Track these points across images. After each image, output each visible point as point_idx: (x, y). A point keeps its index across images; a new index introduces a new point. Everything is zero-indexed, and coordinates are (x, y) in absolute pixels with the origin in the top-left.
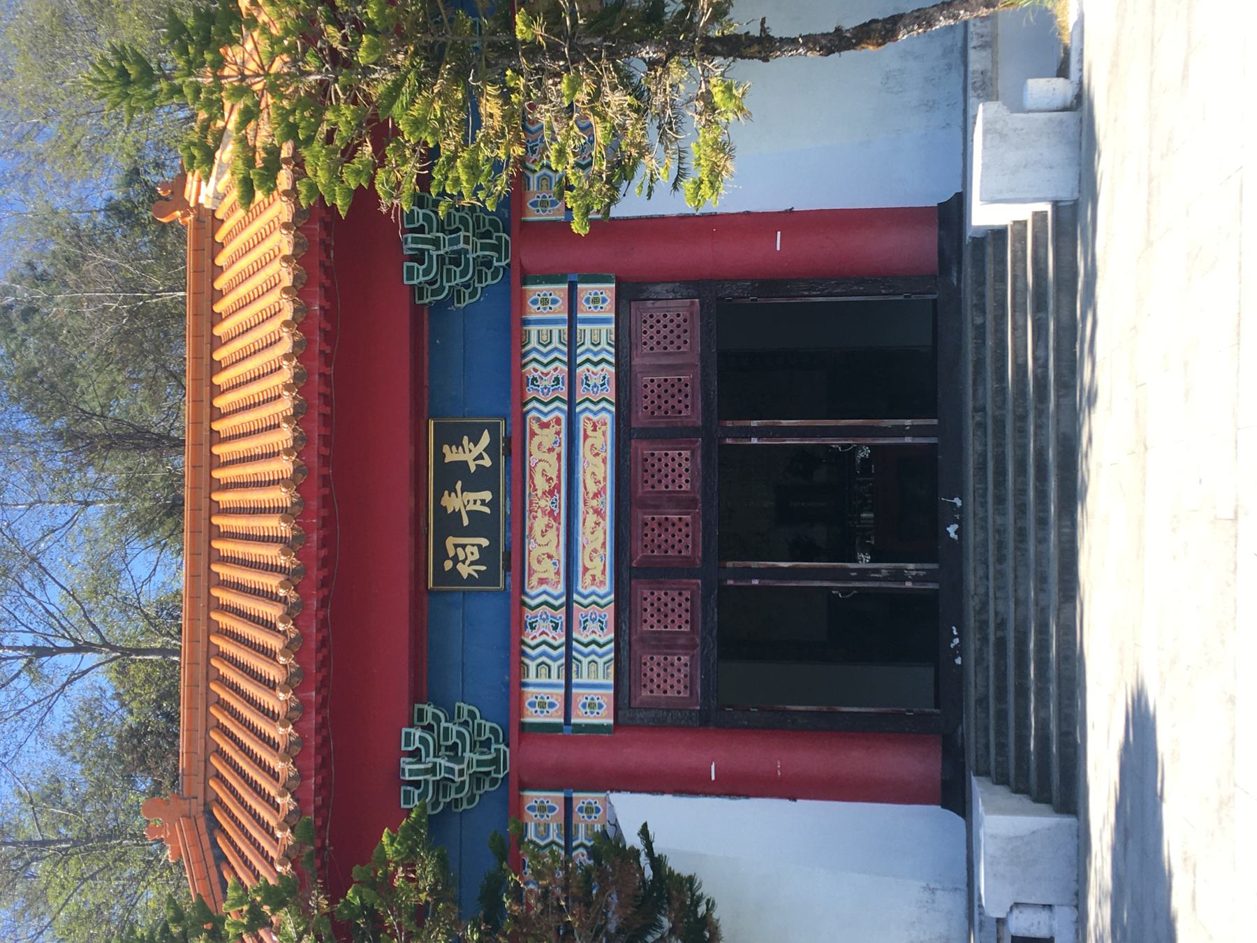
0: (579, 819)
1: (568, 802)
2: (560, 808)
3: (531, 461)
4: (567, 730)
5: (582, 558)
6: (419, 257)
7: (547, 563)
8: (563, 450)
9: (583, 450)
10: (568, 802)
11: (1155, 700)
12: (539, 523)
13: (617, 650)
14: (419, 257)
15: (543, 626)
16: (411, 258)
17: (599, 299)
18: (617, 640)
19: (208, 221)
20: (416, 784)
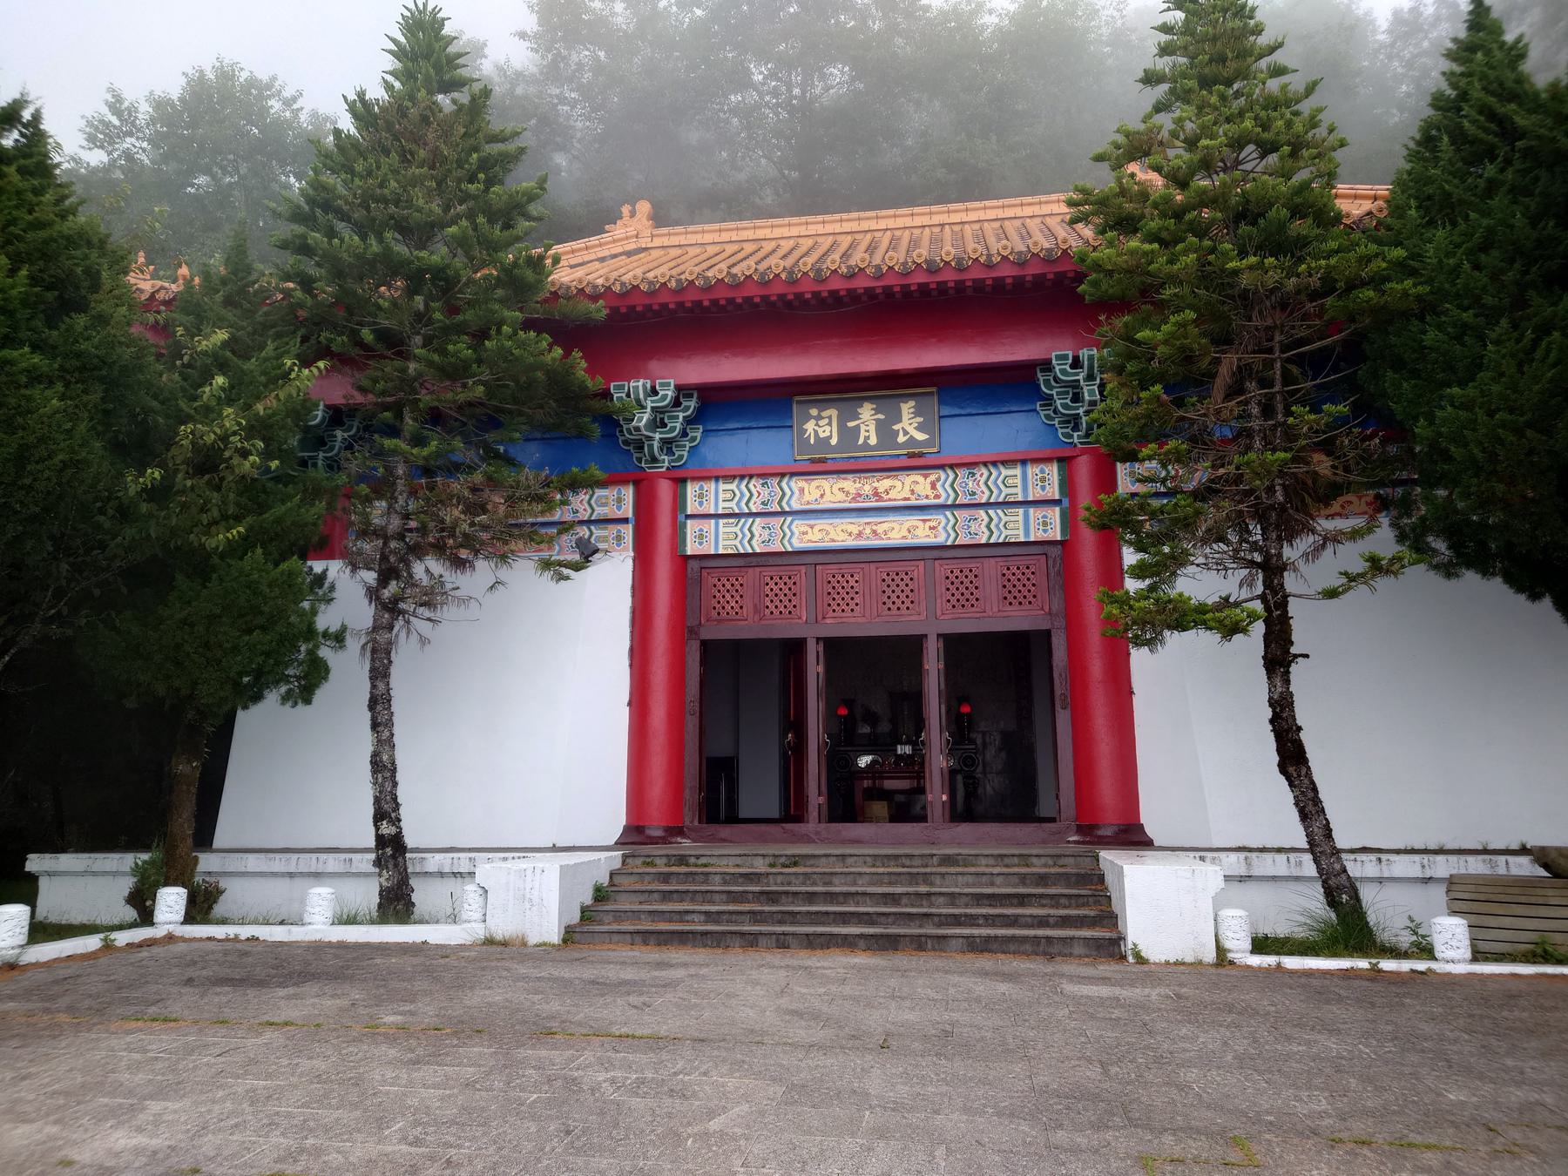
0: (613, 529)
1: (626, 520)
2: (619, 514)
3: (903, 475)
5: (822, 523)
8: (913, 502)
9: (912, 520)
10: (626, 520)
12: (849, 484)
15: (765, 492)
18: (755, 554)
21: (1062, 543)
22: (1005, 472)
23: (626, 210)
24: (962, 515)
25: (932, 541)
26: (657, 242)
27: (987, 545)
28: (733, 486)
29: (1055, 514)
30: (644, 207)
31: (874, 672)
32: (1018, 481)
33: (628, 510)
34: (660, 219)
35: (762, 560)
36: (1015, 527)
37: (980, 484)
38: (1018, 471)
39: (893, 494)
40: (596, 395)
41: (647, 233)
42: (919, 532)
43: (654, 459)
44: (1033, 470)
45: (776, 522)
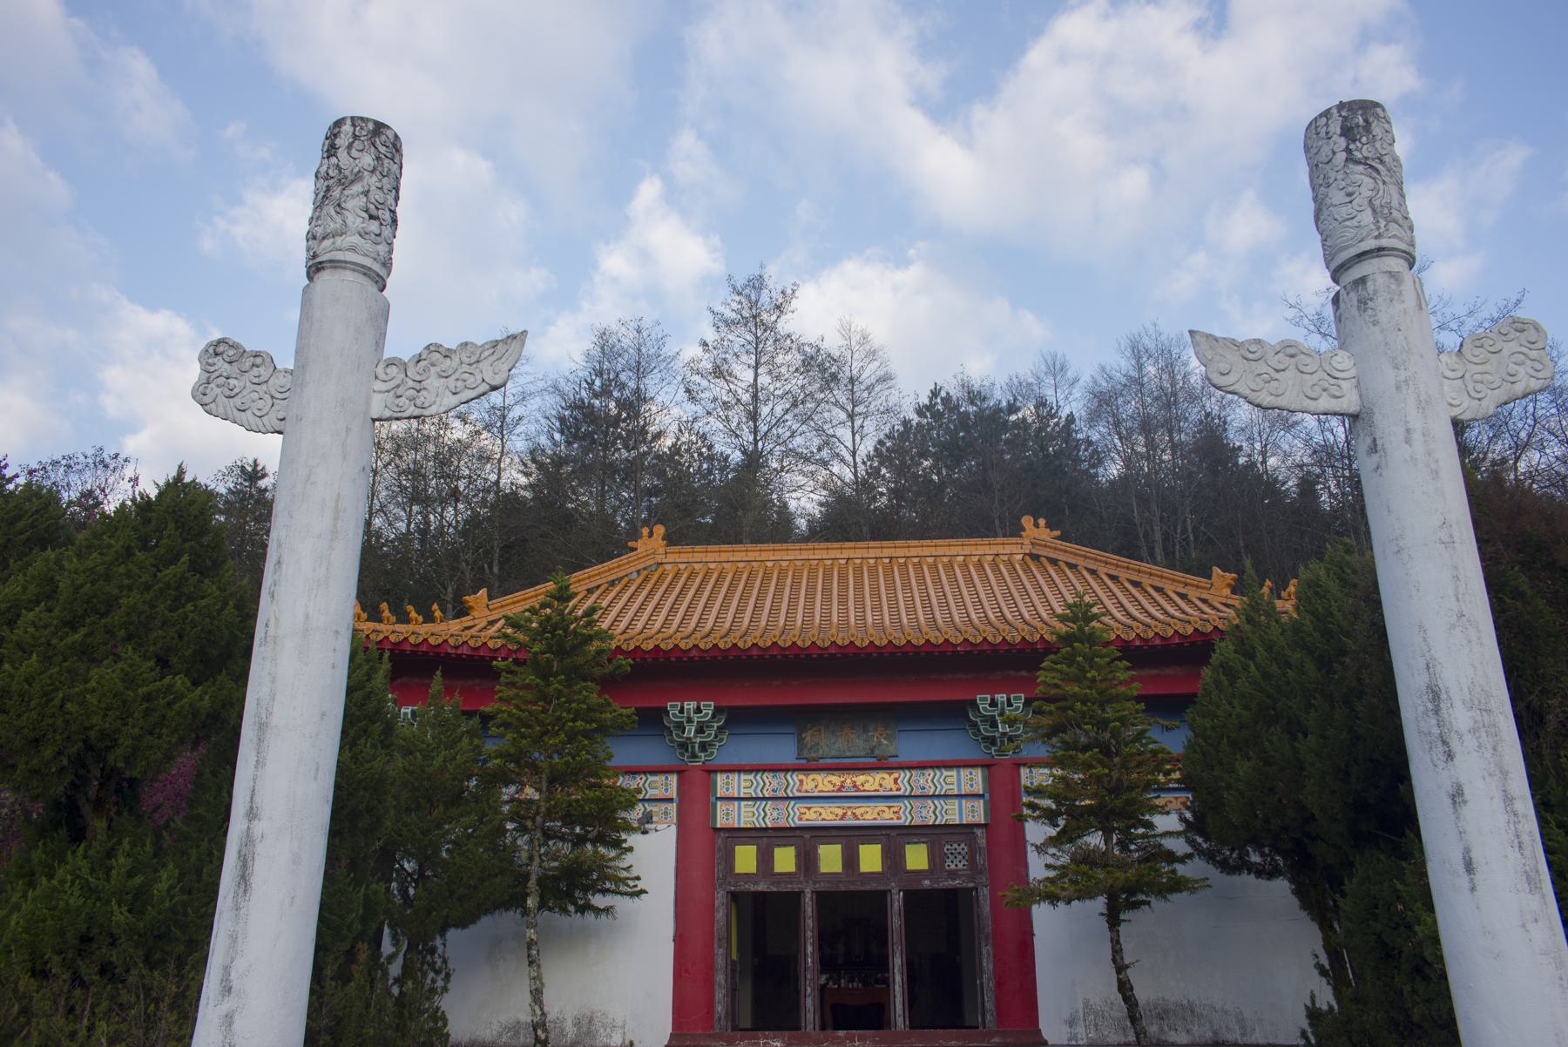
0: (663, 806)
1: (671, 800)
2: (668, 795)
3: (873, 773)
4: (713, 799)
5: (816, 806)
6: (993, 704)
7: (812, 785)
8: (881, 793)
9: (882, 806)
10: (671, 800)
11: (643, 896)
12: (836, 779)
13: (761, 829)
14: (993, 704)
15: (775, 783)
16: (993, 700)
17: (975, 813)
18: (767, 829)
19: (1016, 531)
20: (682, 711)
21: (985, 825)
22: (946, 773)
23: (645, 531)
24: (917, 803)
25: (895, 822)
26: (671, 558)
27: (934, 826)
28: (751, 777)
29: (980, 805)
30: (660, 530)
31: (852, 917)
32: (954, 780)
33: (673, 792)
34: (671, 540)
35: (770, 833)
36: (953, 813)
37: (929, 781)
38: (954, 773)
39: (867, 787)
40: (353, 947)
41: (662, 550)
42: (886, 815)
43: (694, 756)
44: (964, 772)
45: (781, 805)
